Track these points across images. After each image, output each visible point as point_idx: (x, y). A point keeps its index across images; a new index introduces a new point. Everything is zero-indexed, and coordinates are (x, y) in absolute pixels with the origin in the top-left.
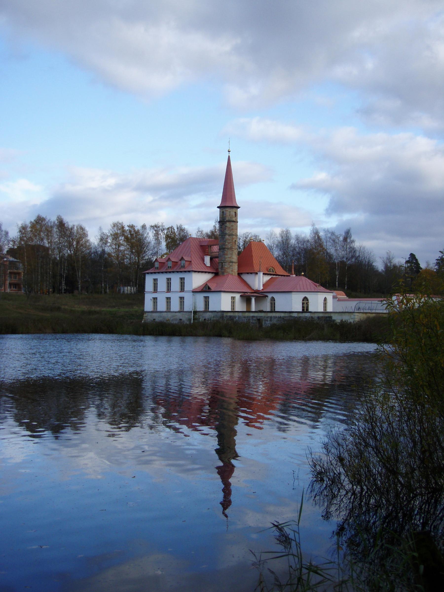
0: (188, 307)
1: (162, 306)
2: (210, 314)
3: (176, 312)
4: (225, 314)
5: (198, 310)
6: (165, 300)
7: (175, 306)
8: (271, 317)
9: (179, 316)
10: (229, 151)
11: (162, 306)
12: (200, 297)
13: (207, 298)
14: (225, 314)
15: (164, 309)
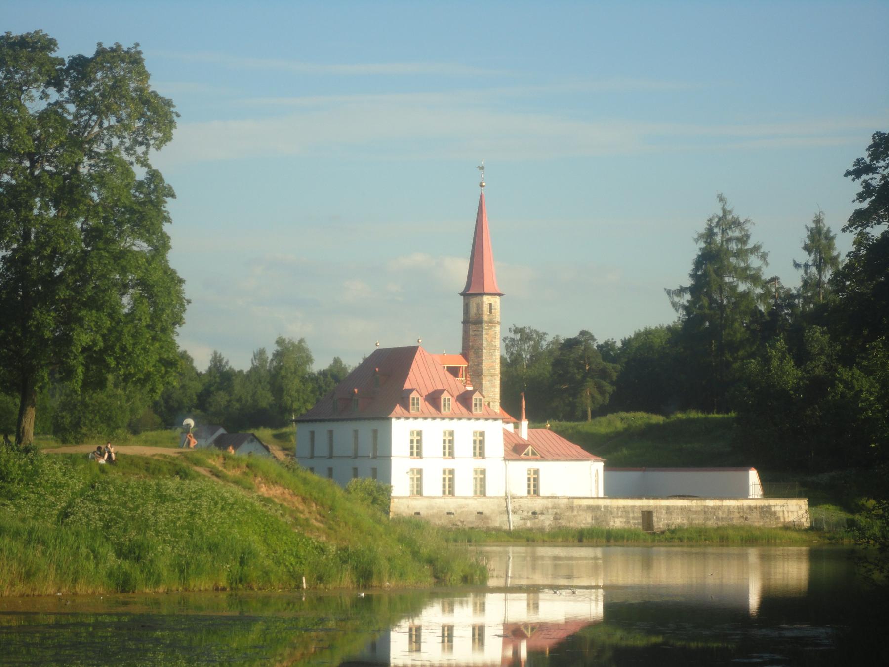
1: (433, 486)
2: (544, 502)
3: (466, 498)
4: (577, 502)
7: (465, 486)
8: (668, 508)
9: (476, 505)
10: (481, 186)
11: (433, 486)
12: (521, 469)
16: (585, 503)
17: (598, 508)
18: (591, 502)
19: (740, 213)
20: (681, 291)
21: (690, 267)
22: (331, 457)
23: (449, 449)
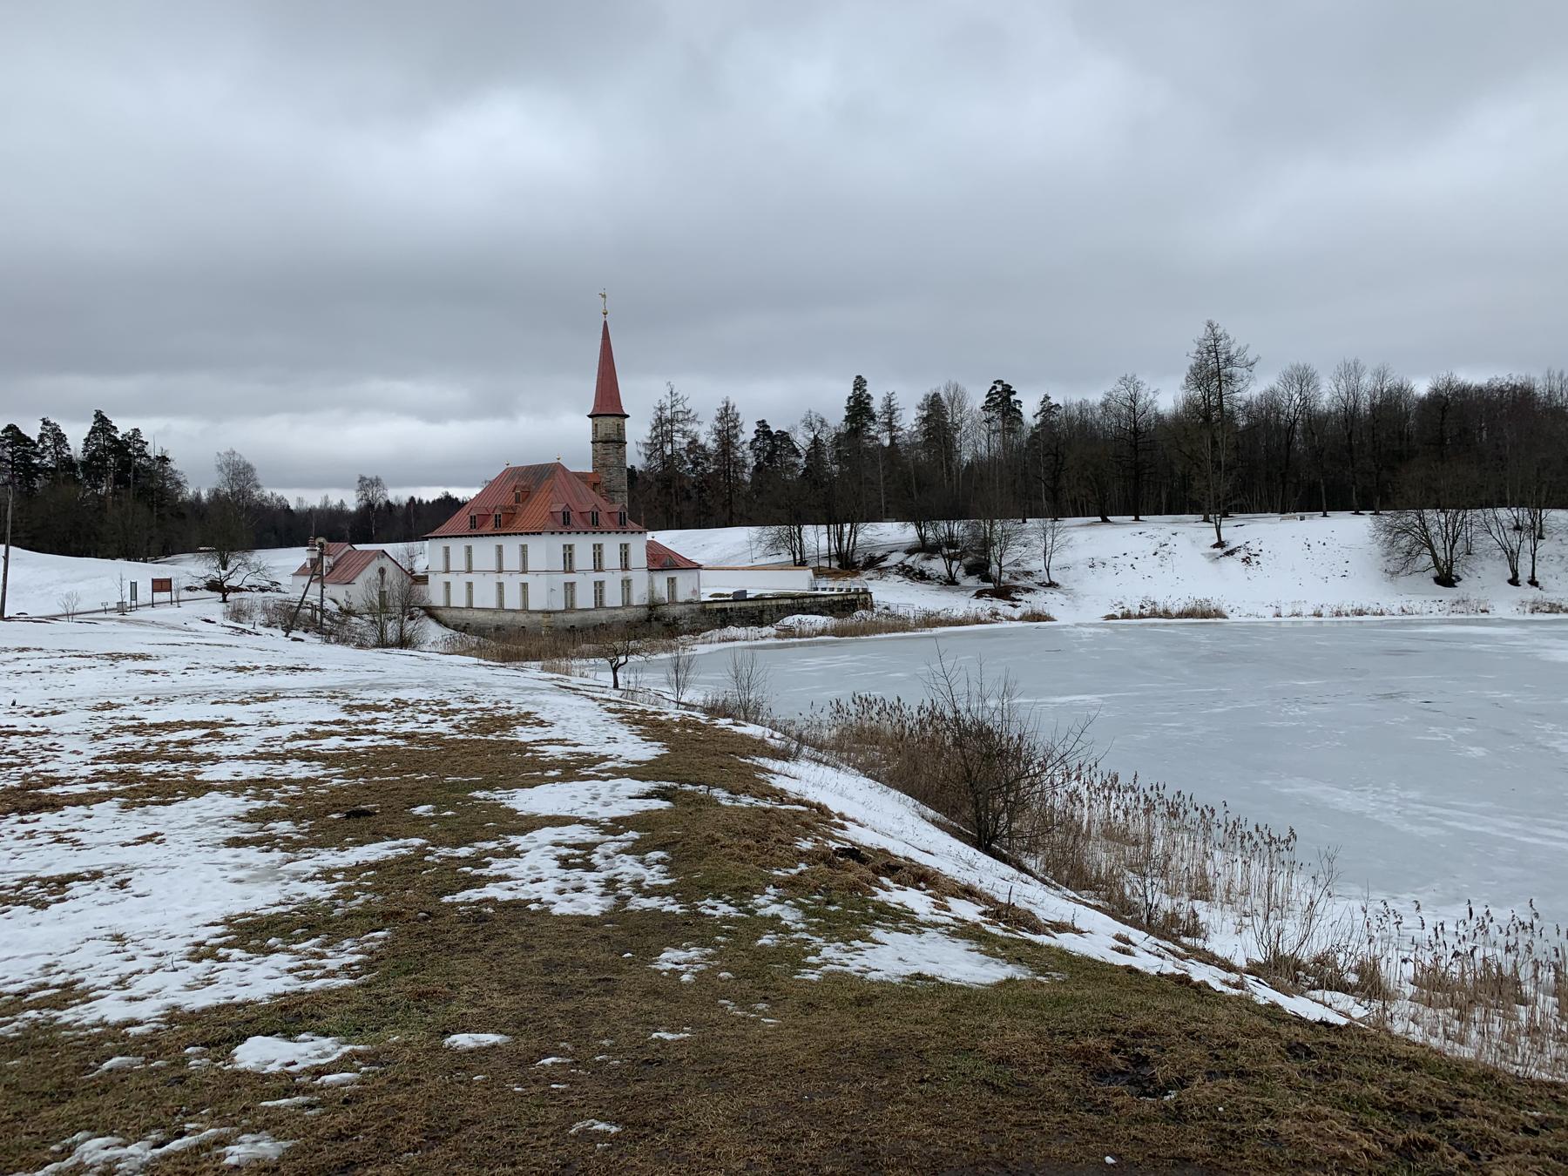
0: (639, 596)
6: (518, 588)
7: (613, 597)
12: (661, 580)
13: (672, 581)
15: (518, 606)
21: (845, 404)
22: (500, 571)
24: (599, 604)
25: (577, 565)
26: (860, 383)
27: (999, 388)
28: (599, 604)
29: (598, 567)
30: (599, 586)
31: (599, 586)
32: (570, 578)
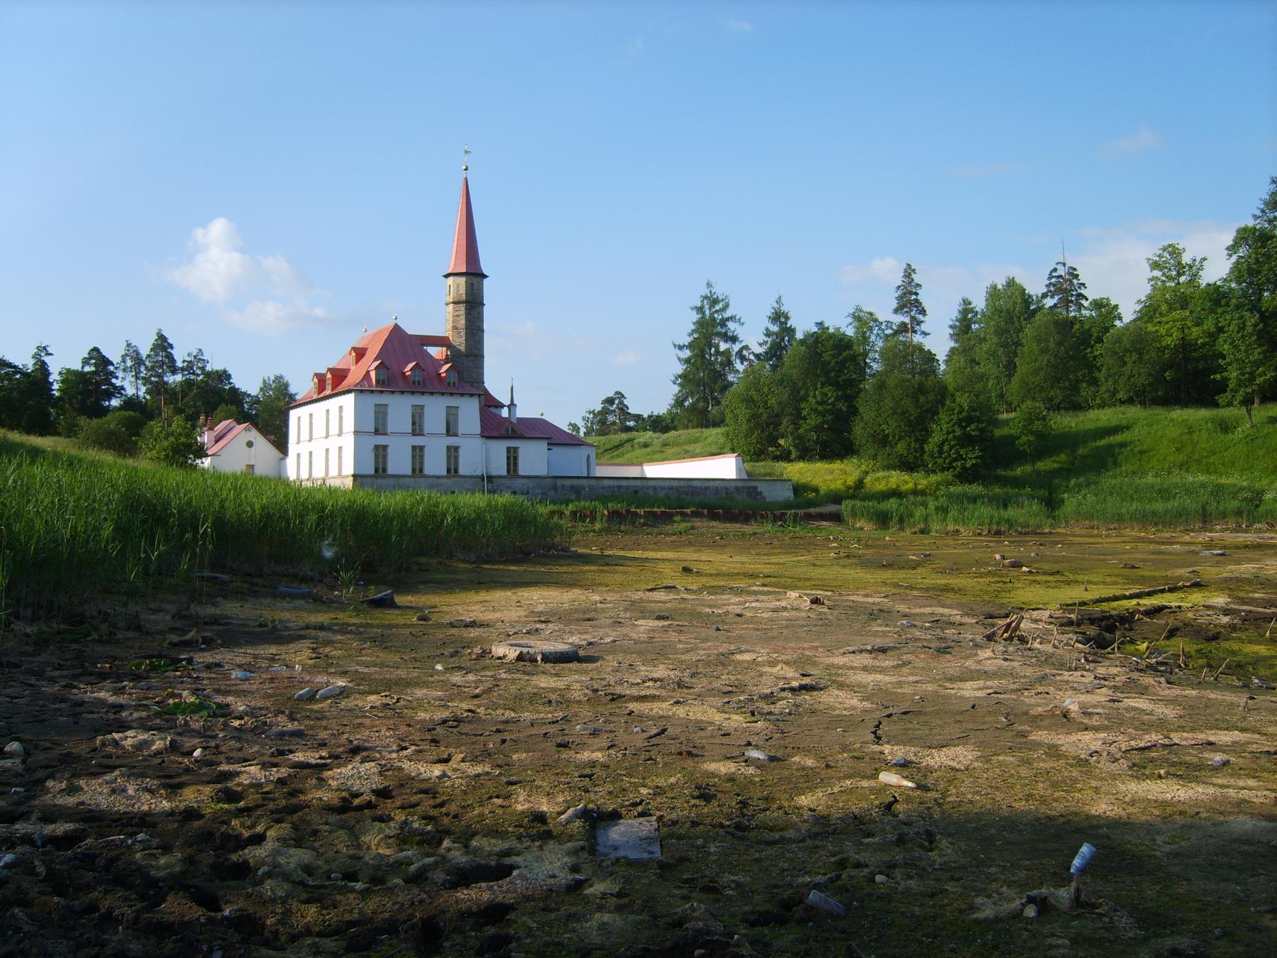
3: (438, 477)
5: (494, 473)
12: (499, 450)
14: (559, 482)
16: (568, 482)
17: (583, 487)
18: (575, 482)
19: (719, 291)
20: (681, 348)
23: (417, 428)
24: (418, 470)
25: (427, 428)
26: (909, 272)
27: (1061, 271)
28: (418, 470)
29: (417, 429)
30: (418, 452)
31: (418, 452)
32: (418, 441)
